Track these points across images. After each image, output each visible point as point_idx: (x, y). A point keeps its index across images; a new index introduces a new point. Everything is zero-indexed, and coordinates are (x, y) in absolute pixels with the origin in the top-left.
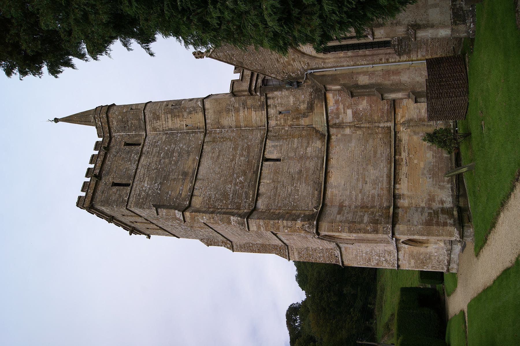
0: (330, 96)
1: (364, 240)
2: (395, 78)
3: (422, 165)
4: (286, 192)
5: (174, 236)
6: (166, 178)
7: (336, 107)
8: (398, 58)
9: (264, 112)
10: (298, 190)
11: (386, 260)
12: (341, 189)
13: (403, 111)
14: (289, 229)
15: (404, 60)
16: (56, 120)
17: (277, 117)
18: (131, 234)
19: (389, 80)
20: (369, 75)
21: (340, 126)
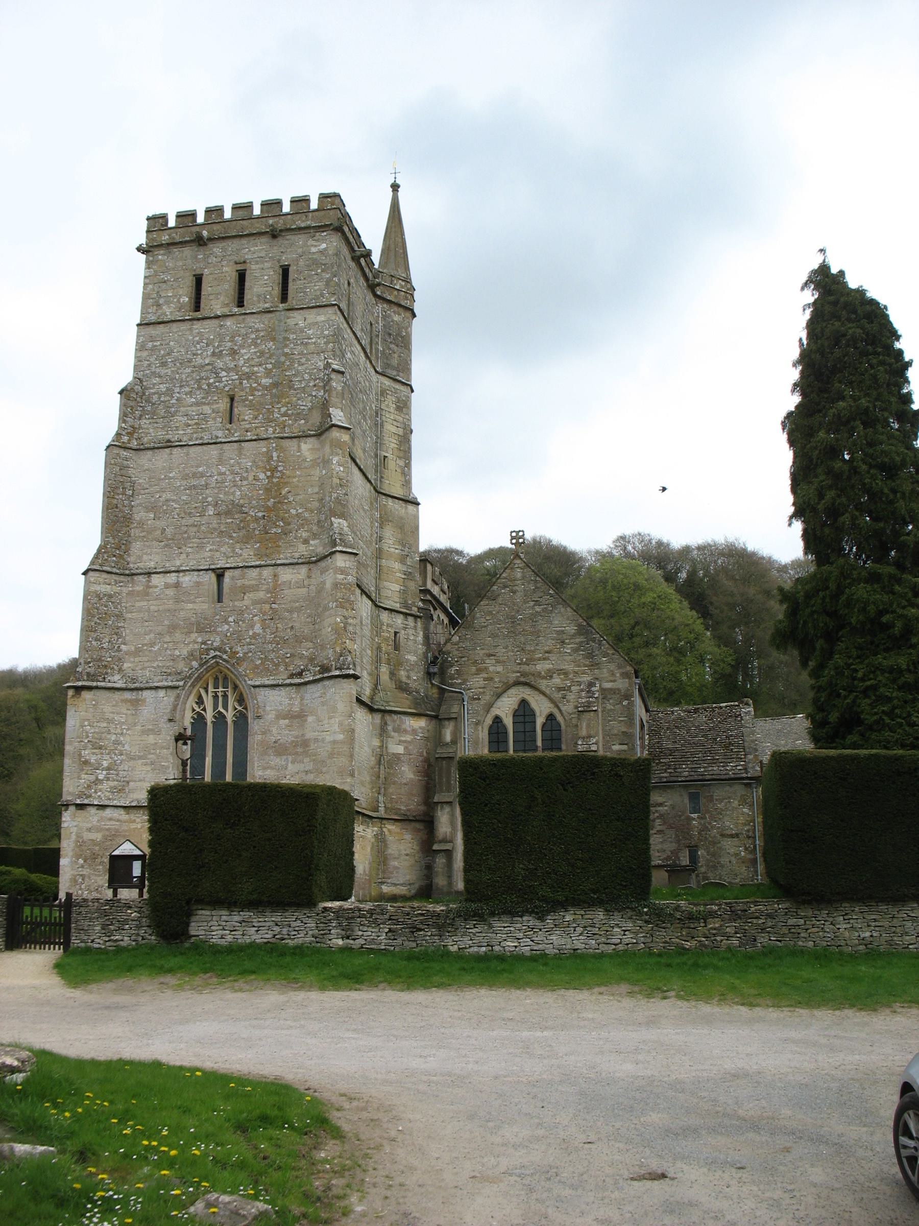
9: (397, 606)
11: (97, 781)
16: (395, 187)
17: (391, 626)
21: (383, 732)
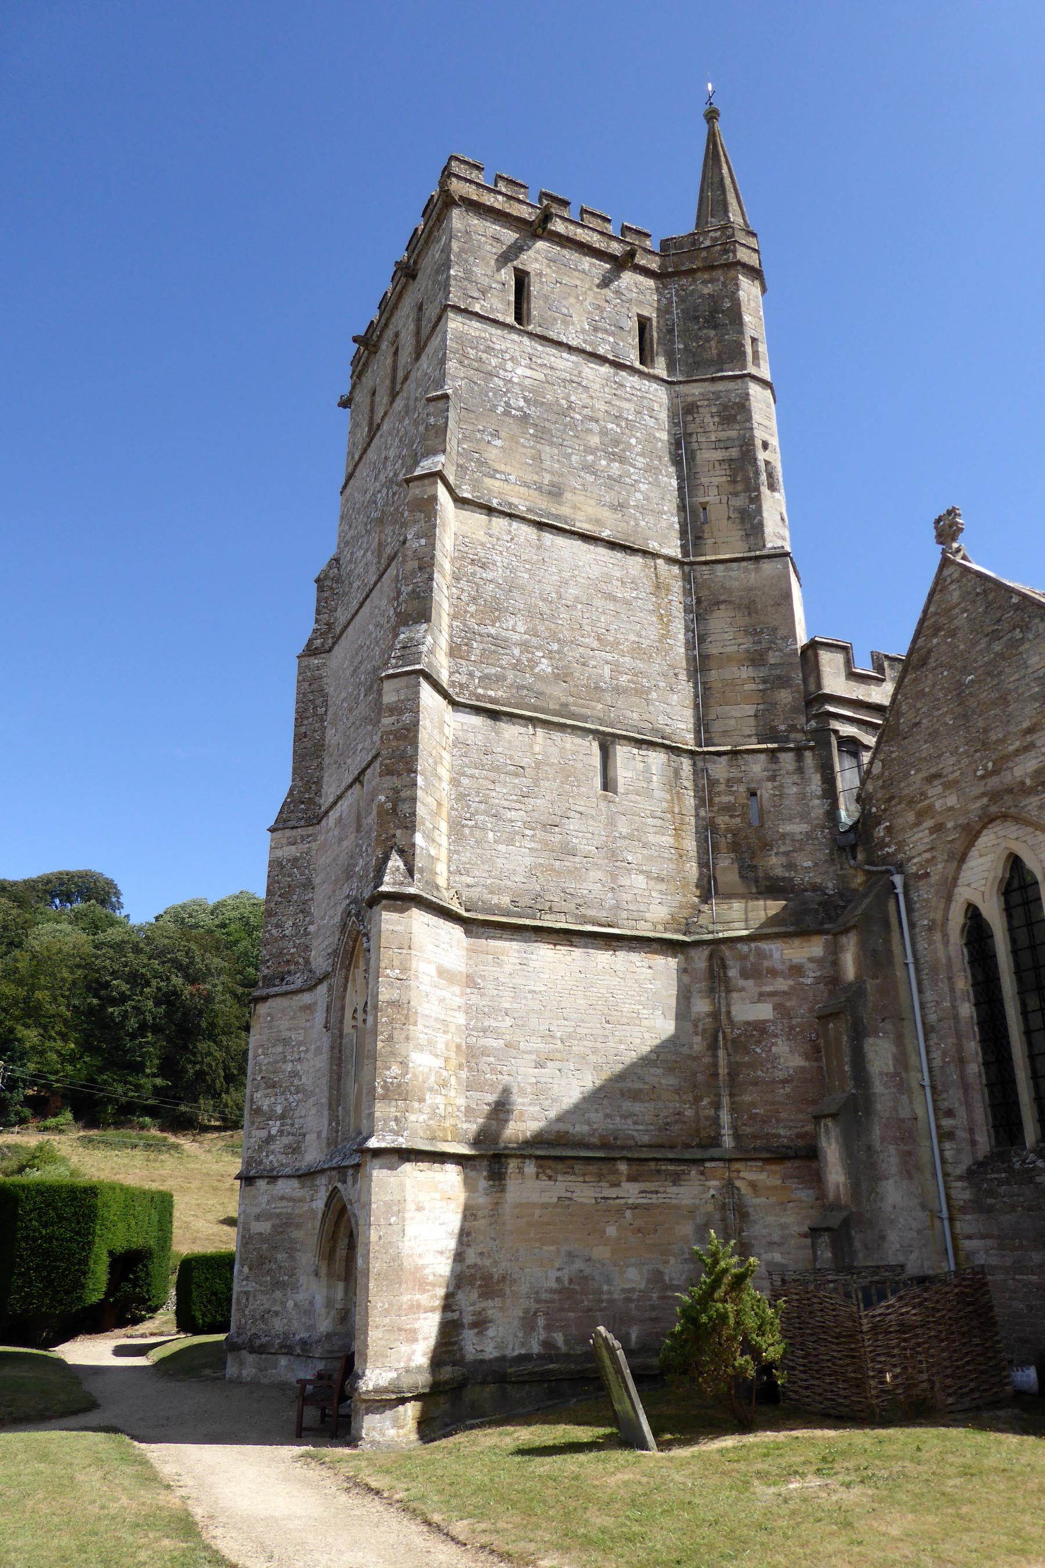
0: (815, 948)
1: (339, 1065)
2: (890, 1159)
3: (601, 1252)
4: (506, 804)
5: (350, 477)
6: (542, 434)
7: (779, 967)
8: (960, 1170)
10: (511, 842)
11: (270, 1139)
12: (518, 981)
13: (775, 1188)
14: (389, 805)
15: (954, 1193)
16: (712, 116)
17: (740, 781)
18: (355, 340)
19: (883, 1140)
20: (897, 1074)
